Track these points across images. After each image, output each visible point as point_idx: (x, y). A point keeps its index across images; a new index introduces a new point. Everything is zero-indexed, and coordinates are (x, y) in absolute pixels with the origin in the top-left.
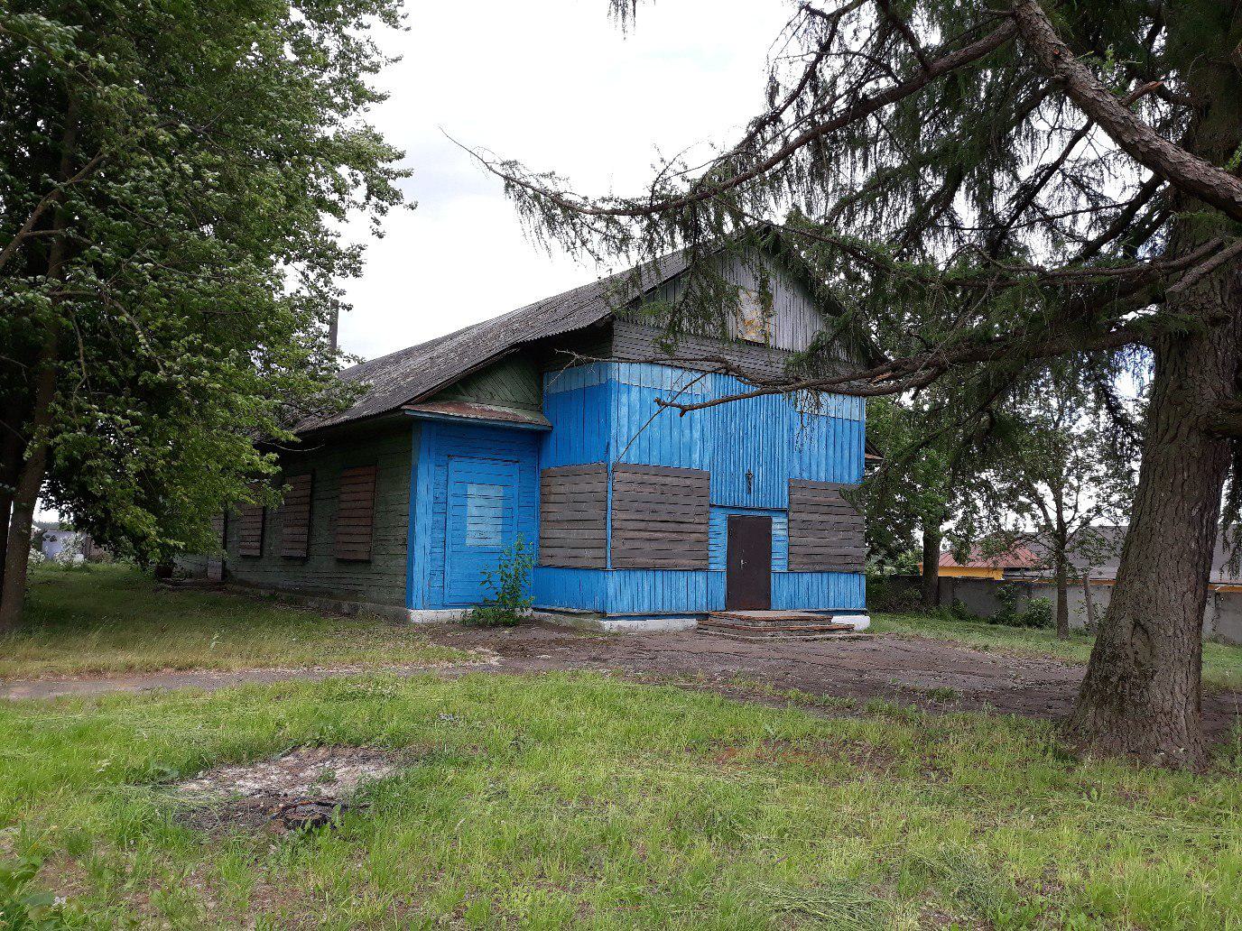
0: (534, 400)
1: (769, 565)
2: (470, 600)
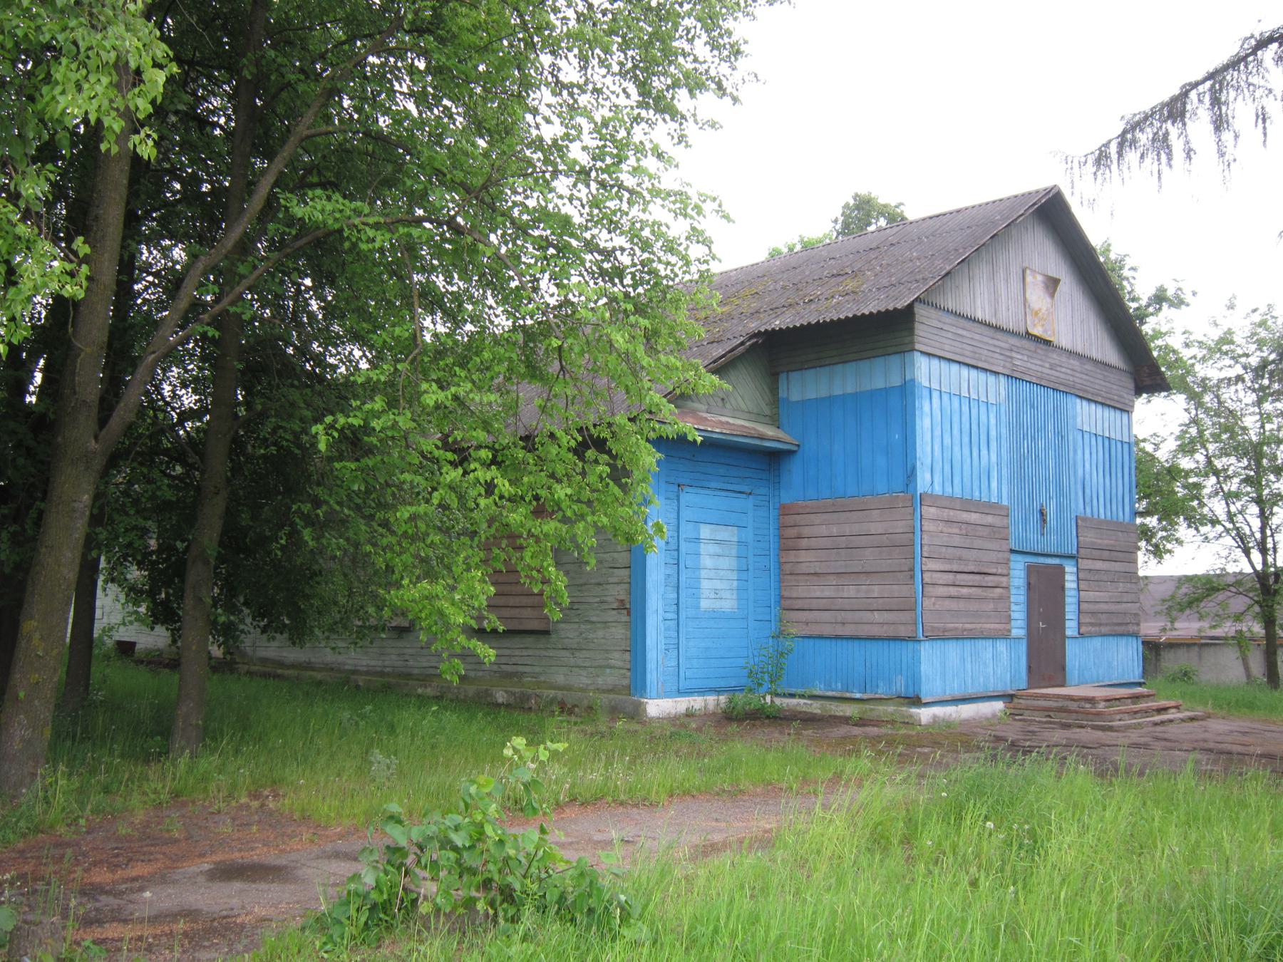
0: (767, 411)
1: (1063, 628)
2: (713, 684)
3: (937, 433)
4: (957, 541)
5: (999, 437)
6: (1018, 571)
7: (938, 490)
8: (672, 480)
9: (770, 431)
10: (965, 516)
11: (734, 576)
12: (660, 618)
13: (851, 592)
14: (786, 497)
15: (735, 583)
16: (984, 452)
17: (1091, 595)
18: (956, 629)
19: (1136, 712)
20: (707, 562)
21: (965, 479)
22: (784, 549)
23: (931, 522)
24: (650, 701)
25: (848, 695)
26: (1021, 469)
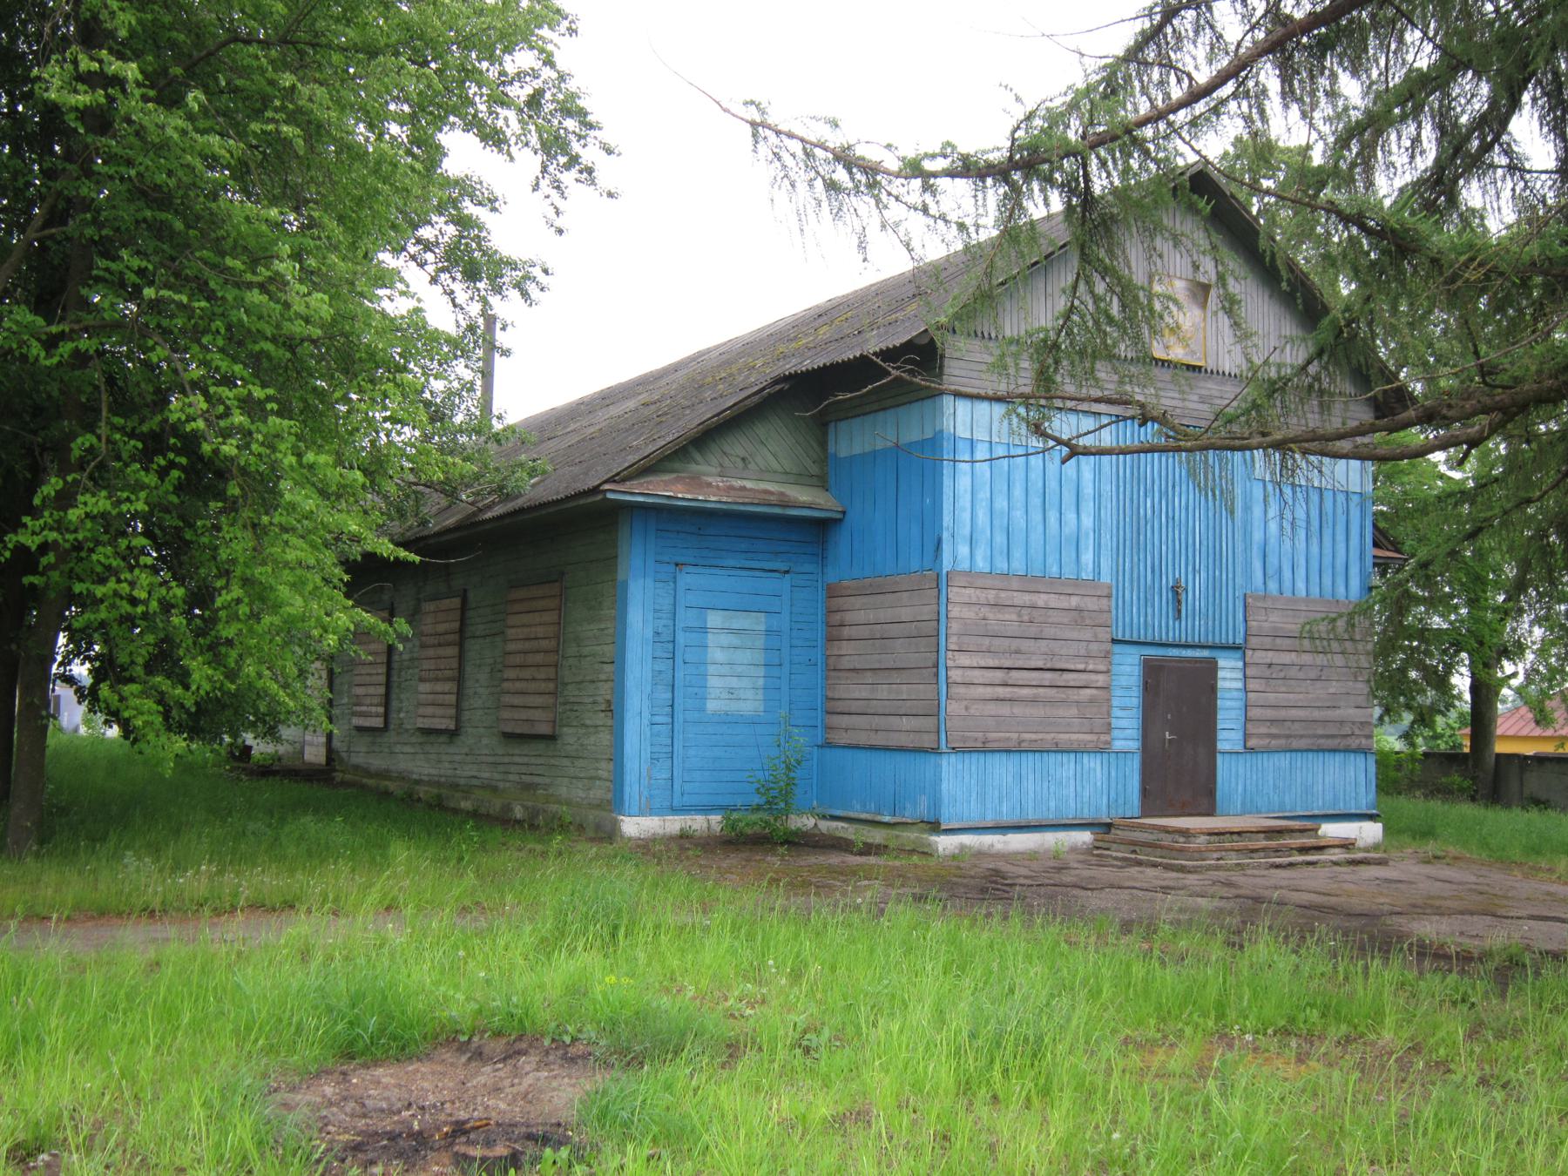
0: (814, 470)
3: (984, 494)
4: (1014, 629)
5: (1098, 497)
6: (1128, 669)
7: (982, 564)
8: (666, 559)
9: (803, 495)
11: (761, 671)
12: (646, 722)
14: (832, 576)
15: (761, 682)
16: (1070, 516)
18: (1008, 739)
19: (1256, 851)
20: (717, 655)
21: (1032, 551)
22: (830, 639)
23: (961, 606)
24: (626, 819)
25: (879, 818)
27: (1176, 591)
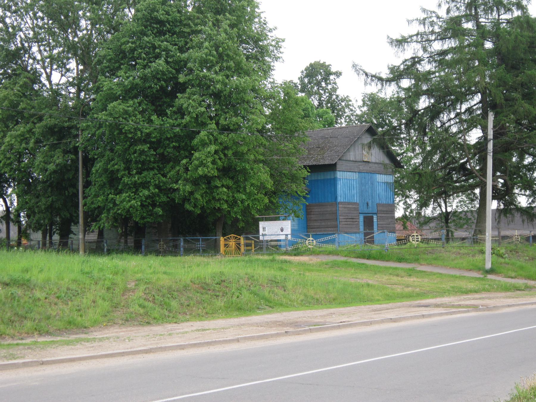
4: (347, 212)
5: (356, 187)
7: (342, 201)
10: (348, 206)
13: (323, 224)
17: (381, 223)
26: (362, 193)
27: (367, 204)
